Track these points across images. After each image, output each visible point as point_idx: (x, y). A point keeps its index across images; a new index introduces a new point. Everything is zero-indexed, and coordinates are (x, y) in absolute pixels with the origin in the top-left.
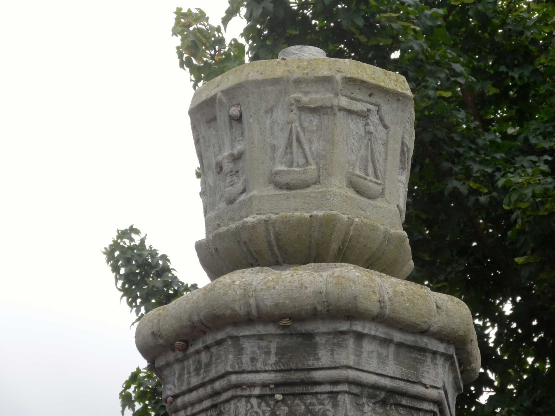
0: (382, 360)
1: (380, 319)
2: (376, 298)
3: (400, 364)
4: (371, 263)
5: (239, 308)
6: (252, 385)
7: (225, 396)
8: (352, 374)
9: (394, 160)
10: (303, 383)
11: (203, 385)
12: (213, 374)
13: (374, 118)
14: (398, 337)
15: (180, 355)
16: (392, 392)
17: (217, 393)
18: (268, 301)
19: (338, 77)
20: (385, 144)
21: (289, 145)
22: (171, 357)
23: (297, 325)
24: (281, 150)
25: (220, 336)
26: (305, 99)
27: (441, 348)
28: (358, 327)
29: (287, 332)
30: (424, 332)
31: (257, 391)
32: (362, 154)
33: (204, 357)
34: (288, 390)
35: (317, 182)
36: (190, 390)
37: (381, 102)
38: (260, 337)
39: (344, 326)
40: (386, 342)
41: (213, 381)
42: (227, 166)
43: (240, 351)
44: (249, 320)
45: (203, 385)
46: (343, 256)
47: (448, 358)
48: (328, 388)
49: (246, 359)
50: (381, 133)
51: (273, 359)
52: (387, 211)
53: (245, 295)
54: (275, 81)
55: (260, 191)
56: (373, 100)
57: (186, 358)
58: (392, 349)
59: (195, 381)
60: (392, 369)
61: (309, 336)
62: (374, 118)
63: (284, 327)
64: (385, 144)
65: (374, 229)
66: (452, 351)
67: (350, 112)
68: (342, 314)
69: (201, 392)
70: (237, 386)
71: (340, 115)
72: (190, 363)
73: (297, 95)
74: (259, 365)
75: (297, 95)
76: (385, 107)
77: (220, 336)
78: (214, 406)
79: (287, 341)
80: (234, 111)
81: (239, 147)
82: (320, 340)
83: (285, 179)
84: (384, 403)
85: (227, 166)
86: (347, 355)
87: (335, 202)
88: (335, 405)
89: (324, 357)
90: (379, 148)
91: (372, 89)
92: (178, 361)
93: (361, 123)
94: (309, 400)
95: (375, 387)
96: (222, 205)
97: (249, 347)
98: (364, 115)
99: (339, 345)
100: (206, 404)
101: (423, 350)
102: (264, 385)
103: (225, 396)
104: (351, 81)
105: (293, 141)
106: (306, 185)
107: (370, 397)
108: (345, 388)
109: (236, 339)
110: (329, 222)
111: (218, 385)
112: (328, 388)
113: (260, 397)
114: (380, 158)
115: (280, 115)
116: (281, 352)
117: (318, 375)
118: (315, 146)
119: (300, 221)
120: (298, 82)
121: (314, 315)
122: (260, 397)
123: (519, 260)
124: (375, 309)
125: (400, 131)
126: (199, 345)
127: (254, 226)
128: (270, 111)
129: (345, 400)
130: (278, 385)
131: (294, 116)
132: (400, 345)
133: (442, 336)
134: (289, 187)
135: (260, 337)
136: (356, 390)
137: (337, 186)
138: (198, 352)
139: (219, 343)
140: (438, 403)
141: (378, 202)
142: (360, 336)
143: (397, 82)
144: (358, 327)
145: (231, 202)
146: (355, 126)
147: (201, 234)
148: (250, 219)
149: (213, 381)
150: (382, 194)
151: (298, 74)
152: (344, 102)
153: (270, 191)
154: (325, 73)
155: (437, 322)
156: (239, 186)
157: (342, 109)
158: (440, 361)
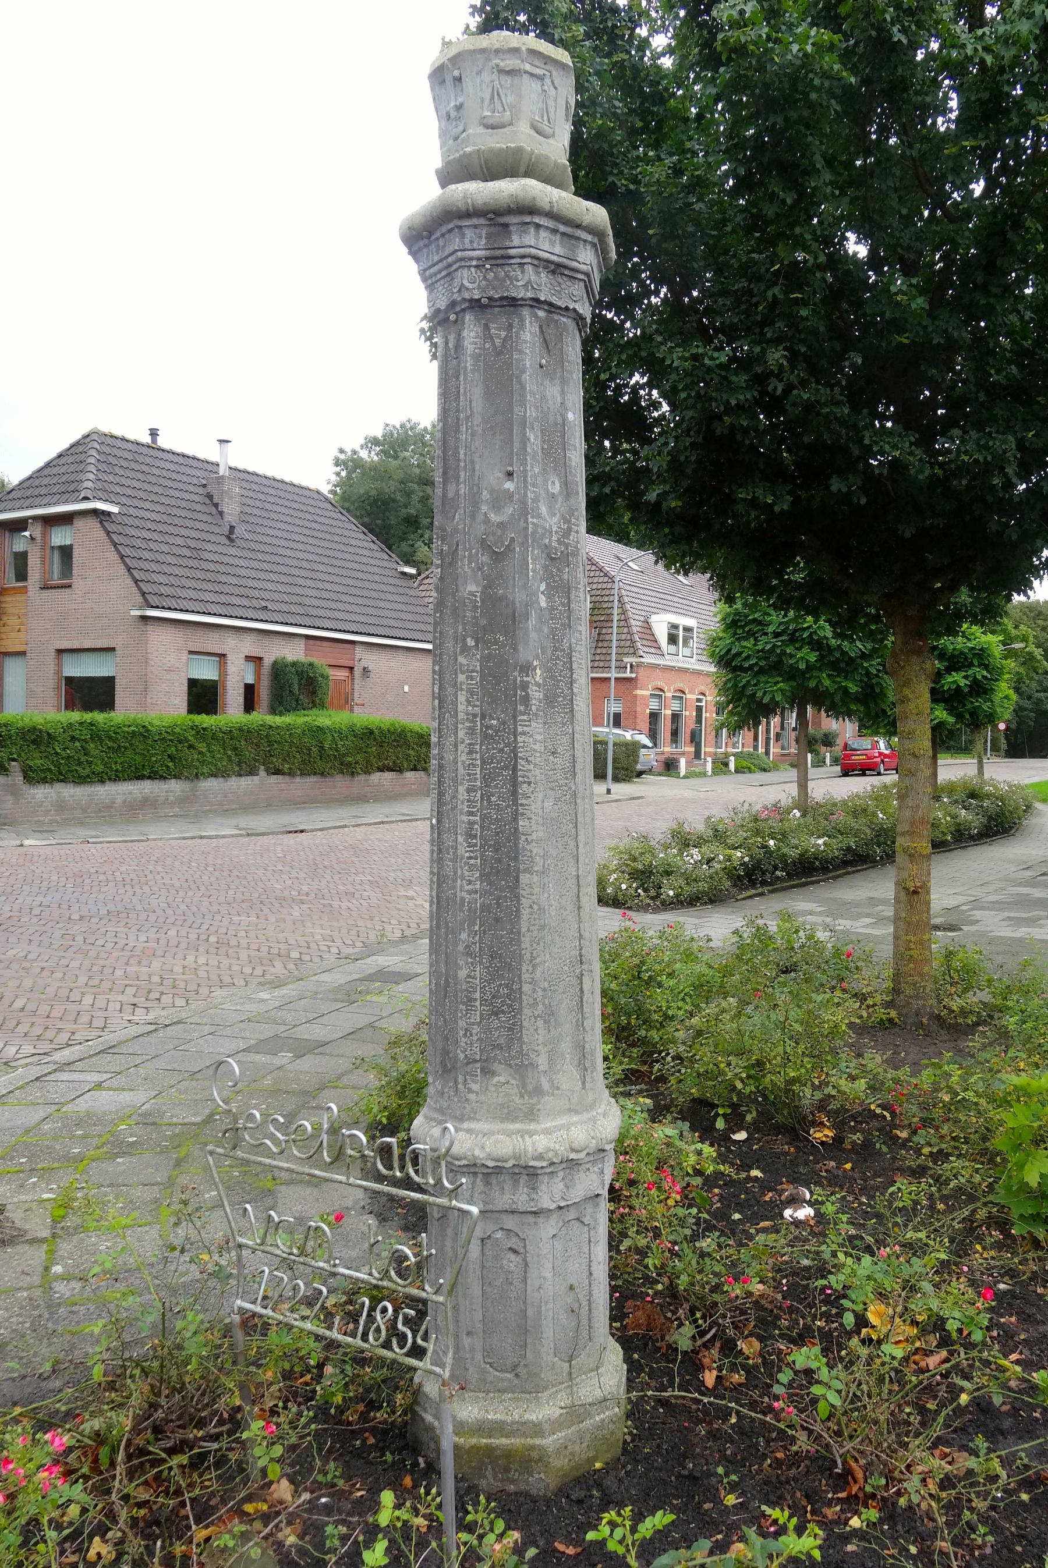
0: (552, 243)
1: (551, 215)
2: (547, 200)
3: (563, 246)
4: (547, 180)
5: (461, 205)
6: (471, 259)
7: (455, 267)
8: (533, 251)
9: (561, 113)
10: (502, 257)
11: (441, 261)
12: (446, 253)
13: (548, 81)
14: (562, 228)
15: (426, 241)
16: (559, 265)
17: (450, 265)
18: (479, 202)
19: (524, 48)
20: (555, 101)
21: (492, 98)
22: (421, 243)
23: (498, 218)
24: (487, 102)
25: (451, 226)
26: (502, 64)
27: (589, 238)
28: (537, 220)
29: (492, 223)
30: (578, 226)
31: (474, 263)
32: (542, 110)
33: (441, 242)
34: (493, 262)
35: (511, 124)
36: (434, 265)
37: (552, 69)
38: (475, 226)
39: (528, 219)
40: (554, 231)
41: (447, 257)
42: (453, 114)
43: (463, 236)
44: (468, 214)
45: (441, 261)
46: (529, 173)
47: (594, 245)
48: (518, 261)
49: (467, 241)
50: (553, 91)
51: (484, 241)
52: (557, 148)
53: (465, 197)
54: (483, 51)
55: (475, 130)
56: (547, 67)
57: (430, 244)
58: (558, 236)
59: (436, 258)
60: (558, 249)
61: (506, 226)
62: (548, 81)
63: (491, 219)
64: (555, 101)
65: (548, 158)
66: (596, 240)
67: (532, 75)
68: (526, 210)
69: (440, 266)
70: (462, 259)
71: (525, 76)
72: (433, 247)
73: (497, 61)
74: (475, 246)
75: (497, 61)
76: (554, 73)
77: (451, 226)
78: (449, 274)
79: (493, 229)
80: (456, 73)
81: (460, 100)
82: (512, 228)
83: (490, 121)
84: (553, 272)
85: (453, 114)
86: (530, 239)
87: (521, 137)
88: (523, 272)
89: (516, 241)
90: (551, 103)
91: (548, 60)
92: (426, 246)
93: (539, 83)
94: (507, 268)
95: (548, 261)
96: (451, 142)
97: (469, 233)
98: (541, 78)
99: (525, 232)
100: (443, 273)
101: (578, 239)
102: (479, 259)
103: (455, 267)
104: (532, 52)
105: (495, 95)
106: (502, 126)
107: (545, 268)
108: (529, 260)
109: (460, 227)
110: (519, 151)
111: (450, 260)
112: (518, 261)
113: (476, 267)
114: (552, 111)
115: (486, 76)
116: (489, 237)
117: (512, 252)
118: (509, 99)
119: (501, 150)
120: (497, 51)
121: (509, 211)
122: (476, 267)
123: (650, 232)
124: (547, 208)
125: (564, 94)
126: (438, 234)
127: (470, 154)
128: (479, 73)
129: (529, 269)
130: (487, 258)
131: (495, 76)
132: (563, 234)
133: (590, 230)
134: (493, 127)
135: (475, 226)
136: (536, 262)
137: (523, 126)
138: (437, 239)
139: (450, 231)
140: (587, 274)
141: (551, 141)
142: (538, 226)
143: (563, 56)
144: (537, 220)
145: (456, 139)
146: (536, 85)
147: (439, 164)
148: (468, 149)
149: (447, 257)
150: (553, 135)
151: (497, 46)
152: (528, 67)
153: (481, 130)
154: (515, 45)
155: (587, 220)
156: (461, 128)
157: (526, 72)
158: (589, 247)
